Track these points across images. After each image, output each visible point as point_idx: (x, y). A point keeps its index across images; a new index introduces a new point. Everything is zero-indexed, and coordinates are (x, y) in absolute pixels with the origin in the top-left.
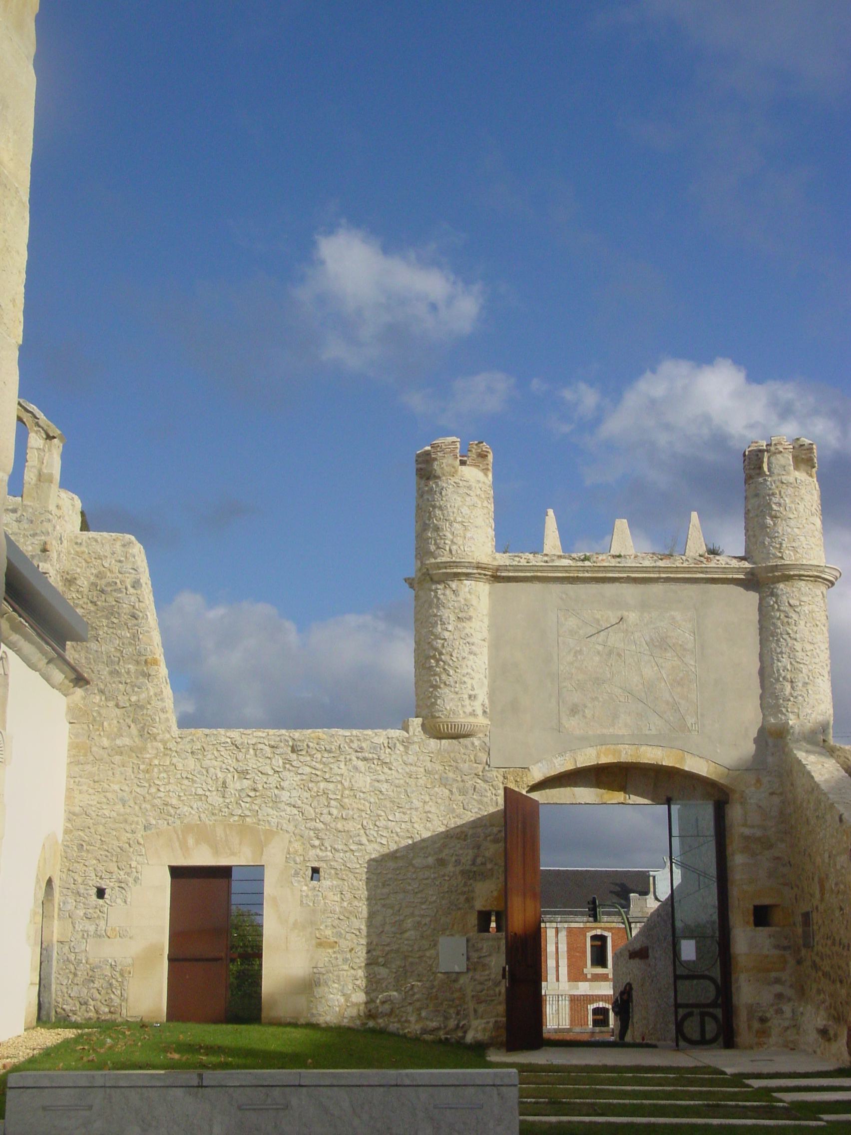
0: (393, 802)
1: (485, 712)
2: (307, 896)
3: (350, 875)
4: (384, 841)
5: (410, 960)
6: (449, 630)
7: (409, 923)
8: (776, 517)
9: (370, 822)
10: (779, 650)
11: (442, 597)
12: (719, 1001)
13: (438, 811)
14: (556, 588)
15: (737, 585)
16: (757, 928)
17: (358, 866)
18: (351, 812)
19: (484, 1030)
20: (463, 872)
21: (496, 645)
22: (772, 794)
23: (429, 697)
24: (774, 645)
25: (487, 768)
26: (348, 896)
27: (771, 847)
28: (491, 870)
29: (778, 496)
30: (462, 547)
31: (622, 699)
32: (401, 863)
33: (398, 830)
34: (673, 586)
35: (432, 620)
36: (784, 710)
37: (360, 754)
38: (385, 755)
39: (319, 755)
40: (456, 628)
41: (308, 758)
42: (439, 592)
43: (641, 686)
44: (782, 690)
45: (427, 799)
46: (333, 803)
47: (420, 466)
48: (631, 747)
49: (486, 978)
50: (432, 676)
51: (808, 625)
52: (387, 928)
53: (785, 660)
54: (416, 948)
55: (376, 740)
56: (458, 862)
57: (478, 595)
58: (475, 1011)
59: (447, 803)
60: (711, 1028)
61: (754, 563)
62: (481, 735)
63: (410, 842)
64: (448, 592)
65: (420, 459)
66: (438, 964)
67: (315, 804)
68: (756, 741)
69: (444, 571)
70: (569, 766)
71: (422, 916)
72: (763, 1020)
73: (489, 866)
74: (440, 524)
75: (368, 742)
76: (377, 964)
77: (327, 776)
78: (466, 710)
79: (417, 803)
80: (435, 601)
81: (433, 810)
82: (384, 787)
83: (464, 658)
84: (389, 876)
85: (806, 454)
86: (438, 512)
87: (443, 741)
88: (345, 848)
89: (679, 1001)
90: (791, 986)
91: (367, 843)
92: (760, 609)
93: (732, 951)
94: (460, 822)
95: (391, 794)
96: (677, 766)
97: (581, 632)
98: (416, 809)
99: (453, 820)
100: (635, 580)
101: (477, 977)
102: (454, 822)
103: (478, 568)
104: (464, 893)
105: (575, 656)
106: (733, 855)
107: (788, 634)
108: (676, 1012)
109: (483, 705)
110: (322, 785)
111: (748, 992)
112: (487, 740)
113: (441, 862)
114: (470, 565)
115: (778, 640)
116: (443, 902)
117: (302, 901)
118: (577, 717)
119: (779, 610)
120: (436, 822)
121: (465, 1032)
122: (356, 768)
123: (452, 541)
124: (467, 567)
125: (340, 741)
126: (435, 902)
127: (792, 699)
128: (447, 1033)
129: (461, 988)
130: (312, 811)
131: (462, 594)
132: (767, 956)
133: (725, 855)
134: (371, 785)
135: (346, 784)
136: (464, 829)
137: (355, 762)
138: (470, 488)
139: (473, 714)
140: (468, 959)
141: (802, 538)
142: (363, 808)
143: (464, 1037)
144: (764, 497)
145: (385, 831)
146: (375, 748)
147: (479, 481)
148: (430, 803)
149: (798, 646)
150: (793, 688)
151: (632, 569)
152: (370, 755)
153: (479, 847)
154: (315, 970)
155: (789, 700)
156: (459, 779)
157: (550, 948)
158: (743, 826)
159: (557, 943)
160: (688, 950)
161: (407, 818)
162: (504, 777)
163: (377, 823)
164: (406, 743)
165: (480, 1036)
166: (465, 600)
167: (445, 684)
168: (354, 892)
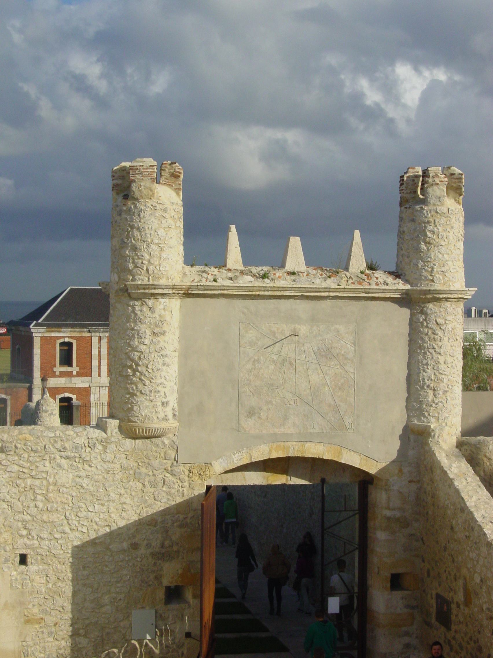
0: (93, 495)
1: (174, 415)
2: (16, 580)
3: (55, 560)
4: (85, 530)
5: (107, 630)
6: (145, 344)
7: (106, 599)
9: (72, 513)
10: (425, 362)
11: (139, 313)
12: (356, 645)
13: (132, 503)
16: (393, 592)
17: (62, 552)
18: (55, 505)
20: (153, 555)
21: (185, 355)
22: (410, 482)
26: (53, 578)
28: (178, 551)
29: (432, 224)
30: (158, 268)
31: (292, 403)
33: (97, 520)
34: (339, 303)
36: (426, 414)
37: (63, 453)
39: (26, 455)
40: (152, 342)
41: (16, 458)
42: (137, 308)
43: (308, 391)
44: (426, 397)
45: (123, 492)
46: (39, 497)
47: (116, 182)
48: (297, 443)
50: (129, 384)
51: (450, 341)
53: (430, 371)
54: (112, 619)
55: (78, 440)
56: (148, 545)
59: (140, 495)
61: (407, 281)
62: (171, 435)
63: (108, 530)
65: (116, 175)
67: (22, 498)
68: (401, 437)
69: (143, 291)
71: (117, 593)
73: (175, 548)
74: (138, 244)
75: (71, 442)
76: (79, 635)
77: (34, 473)
80: (133, 315)
81: (128, 501)
82: (85, 482)
83: (158, 370)
85: (455, 183)
86: (136, 233)
87: (137, 441)
88: (50, 537)
90: (416, 637)
91: (69, 531)
92: (410, 324)
94: (151, 511)
95: (91, 488)
96: (335, 459)
97: (259, 343)
98: (113, 501)
99: (145, 510)
100: (308, 298)
102: (147, 512)
103: (173, 289)
104: (154, 572)
105: (254, 364)
107: (434, 348)
109: (173, 409)
110: (29, 481)
113: (135, 546)
114: (167, 287)
115: (425, 353)
116: (136, 580)
117: (11, 585)
118: (253, 418)
119: (427, 327)
120: (131, 512)
122: (60, 466)
123: (149, 261)
124: (163, 289)
125: (46, 441)
127: (434, 405)
130: (20, 506)
133: (367, 527)
135: (51, 480)
137: (59, 460)
138: (165, 210)
139: (165, 419)
141: (450, 263)
142: (66, 501)
144: (420, 224)
147: (173, 203)
148: (125, 496)
149: (441, 359)
150: (435, 395)
151: (306, 289)
152: (73, 454)
153: (167, 531)
154: (24, 644)
155: (431, 406)
156: (151, 473)
157: (95, 352)
158: (386, 509)
159: (100, 348)
161: (105, 509)
162: (190, 471)
163: (79, 514)
164: (105, 443)
166: (160, 316)
168: (57, 574)
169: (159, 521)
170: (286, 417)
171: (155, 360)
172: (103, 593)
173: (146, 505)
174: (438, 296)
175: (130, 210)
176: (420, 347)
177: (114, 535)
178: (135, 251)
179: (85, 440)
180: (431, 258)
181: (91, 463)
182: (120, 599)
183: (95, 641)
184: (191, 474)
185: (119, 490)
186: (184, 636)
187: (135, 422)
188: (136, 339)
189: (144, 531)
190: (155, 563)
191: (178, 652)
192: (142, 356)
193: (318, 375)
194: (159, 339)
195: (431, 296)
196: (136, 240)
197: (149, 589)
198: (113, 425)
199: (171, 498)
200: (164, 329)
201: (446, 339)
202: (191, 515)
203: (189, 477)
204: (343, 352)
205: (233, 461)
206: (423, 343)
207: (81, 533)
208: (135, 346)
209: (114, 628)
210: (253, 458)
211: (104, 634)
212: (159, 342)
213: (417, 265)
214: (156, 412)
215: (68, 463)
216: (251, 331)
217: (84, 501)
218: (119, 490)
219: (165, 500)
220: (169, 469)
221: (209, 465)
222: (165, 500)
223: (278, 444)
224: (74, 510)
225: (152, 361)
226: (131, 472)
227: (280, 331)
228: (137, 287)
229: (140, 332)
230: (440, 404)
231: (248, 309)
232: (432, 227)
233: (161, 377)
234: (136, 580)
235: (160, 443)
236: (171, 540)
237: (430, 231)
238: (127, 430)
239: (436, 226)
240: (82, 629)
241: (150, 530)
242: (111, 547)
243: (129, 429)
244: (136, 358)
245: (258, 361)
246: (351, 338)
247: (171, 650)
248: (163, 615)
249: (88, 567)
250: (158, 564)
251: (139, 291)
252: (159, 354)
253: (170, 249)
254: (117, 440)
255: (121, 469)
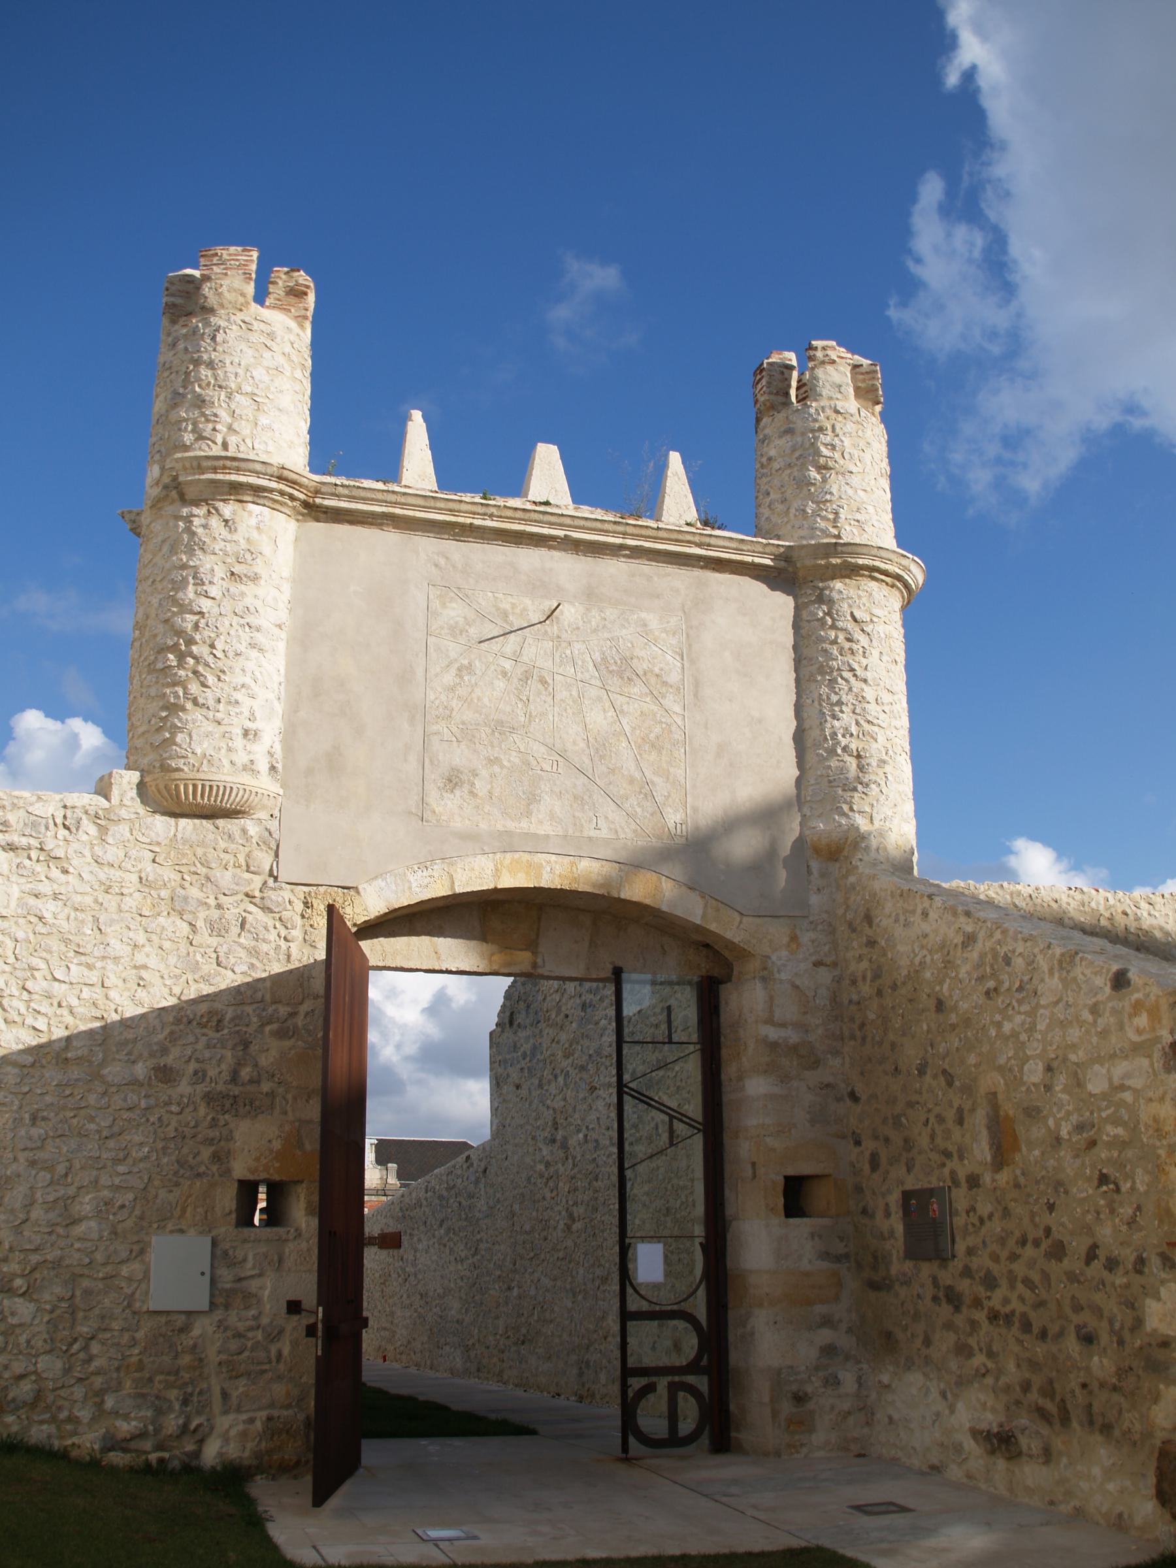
0: (66, 942)
1: (273, 768)
4: (41, 1024)
5: (86, 1283)
7: (86, 1204)
8: (826, 468)
10: (834, 698)
11: (200, 531)
12: (704, 1362)
13: (162, 967)
14: (427, 545)
15: (757, 577)
16: (791, 1220)
19: (244, 1435)
20: (209, 1098)
21: (304, 637)
22: (818, 964)
23: (159, 729)
24: (824, 690)
25: (271, 881)
27: (816, 1064)
28: (272, 1095)
29: (829, 432)
32: (75, 1073)
33: (74, 1002)
35: (177, 576)
36: (845, 808)
38: (55, 841)
42: (196, 521)
43: (582, 745)
45: (141, 938)
49: (250, 1323)
50: (168, 685)
52: (37, 1213)
53: (847, 718)
54: (99, 1257)
55: (38, 809)
56: (199, 1076)
57: (270, 536)
58: (225, 1395)
59: (183, 952)
60: (689, 1414)
64: (214, 522)
65: (173, 289)
66: (147, 1293)
70: (439, 890)
71: (118, 1188)
72: (800, 1399)
73: (266, 1087)
78: (235, 758)
79: (118, 948)
81: (153, 962)
82: (49, 908)
84: (48, 1099)
86: (204, 372)
87: (183, 822)
89: (631, 1362)
90: (849, 1330)
92: (796, 626)
93: (729, 1264)
95: (64, 923)
97: (472, 631)
98: (116, 959)
101: (233, 1319)
103: (280, 478)
104: (210, 1141)
106: (740, 1078)
107: (852, 670)
108: (624, 1387)
109: (271, 754)
111: (769, 1345)
112: (273, 825)
113: (165, 1074)
115: (833, 681)
118: (457, 792)
119: (833, 627)
121: (201, 1442)
123: (230, 428)
124: (257, 473)
126: (146, 1158)
127: (860, 787)
128: (160, 1447)
129: (195, 1346)
131: (242, 528)
132: (807, 1274)
134: (21, 903)
136: (218, 1006)
138: (271, 336)
139: (250, 768)
140: (213, 1282)
141: (871, 509)
143: (197, 1454)
145: (46, 1002)
146: (34, 825)
148: (147, 949)
149: (869, 693)
153: (246, 1045)
156: (212, 902)
158: (765, 1023)
160: (649, 1262)
161: (94, 977)
163: (29, 985)
164: (104, 823)
165: (233, 1451)
167: (195, 702)
169: (228, 1016)
170: (533, 799)
171: (232, 632)
172: (79, 1188)
173: (196, 977)
174: (853, 560)
175: (195, 331)
176: (822, 670)
177: (110, 1039)
178: (200, 407)
179: (56, 810)
180: (831, 493)
181: (66, 865)
182: (123, 1206)
183: (52, 1312)
184: (309, 911)
185: (131, 934)
186: (284, 1310)
187: (178, 770)
188: (191, 588)
189: (191, 1039)
190: (213, 1119)
191: (268, 1352)
192: (202, 621)
193: (604, 711)
194: (243, 587)
195: (839, 561)
196: (204, 385)
197: (198, 1184)
198: (125, 781)
199: (258, 964)
200: (257, 569)
201: (875, 653)
202: (304, 1008)
203: (303, 916)
204: (657, 670)
205: (410, 888)
206: (827, 661)
207: (32, 1032)
208: (187, 602)
209: (104, 1279)
210: (456, 884)
211: (78, 1293)
212: (243, 594)
213: (804, 511)
214: (229, 750)
215: (10, 862)
216: (454, 605)
217: (44, 955)
218: (131, 934)
219: (245, 968)
220: (257, 894)
221: (352, 892)
222: (245, 968)
223: (517, 855)
224: (19, 973)
225: (225, 634)
226: (164, 893)
227: (518, 611)
228: (199, 466)
229: (202, 570)
230: (873, 786)
231: (447, 558)
232: (828, 438)
233: (243, 670)
234: (165, 1160)
235: (237, 834)
236: (256, 1065)
237: (826, 445)
238: (159, 792)
239: (837, 436)
240: (23, 1276)
241: (204, 1038)
242: (105, 1072)
243: (162, 787)
244: (189, 627)
245: (469, 668)
246: (674, 642)
247: (249, 1344)
248: (231, 1252)
249: (44, 1119)
250: (222, 1123)
251: (202, 477)
252: (242, 621)
253: (277, 413)
254: (133, 816)
255: (139, 885)
